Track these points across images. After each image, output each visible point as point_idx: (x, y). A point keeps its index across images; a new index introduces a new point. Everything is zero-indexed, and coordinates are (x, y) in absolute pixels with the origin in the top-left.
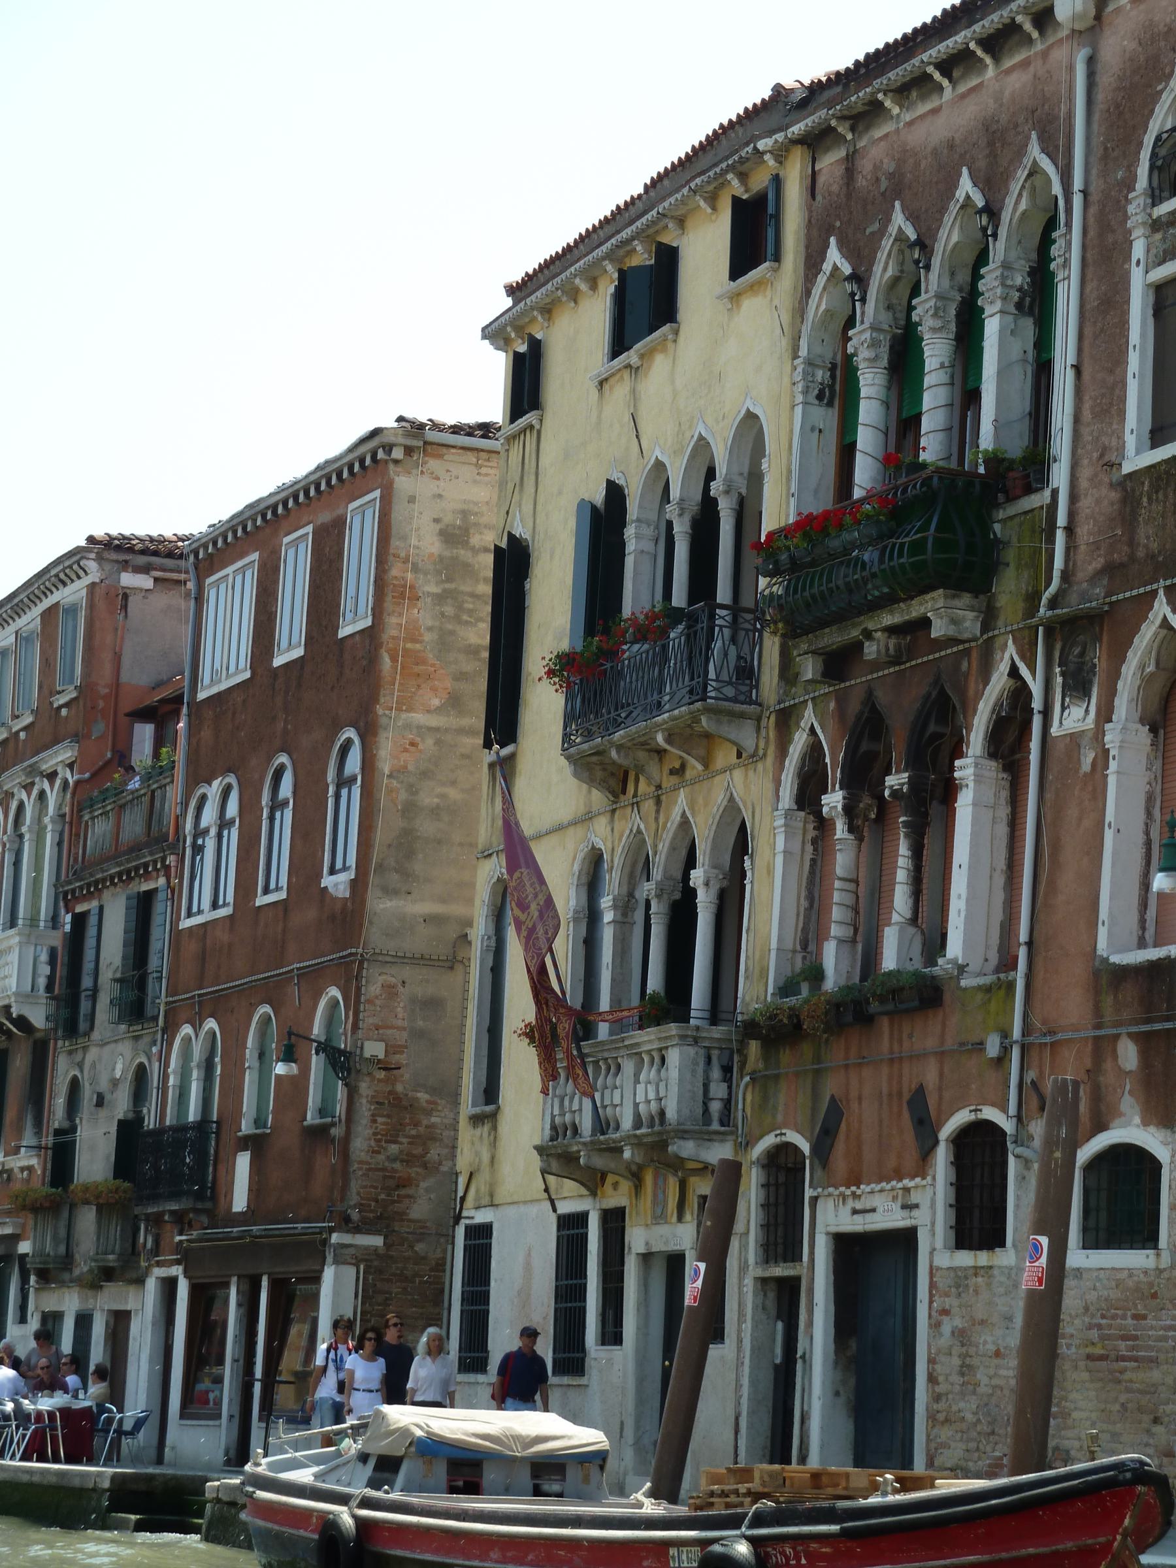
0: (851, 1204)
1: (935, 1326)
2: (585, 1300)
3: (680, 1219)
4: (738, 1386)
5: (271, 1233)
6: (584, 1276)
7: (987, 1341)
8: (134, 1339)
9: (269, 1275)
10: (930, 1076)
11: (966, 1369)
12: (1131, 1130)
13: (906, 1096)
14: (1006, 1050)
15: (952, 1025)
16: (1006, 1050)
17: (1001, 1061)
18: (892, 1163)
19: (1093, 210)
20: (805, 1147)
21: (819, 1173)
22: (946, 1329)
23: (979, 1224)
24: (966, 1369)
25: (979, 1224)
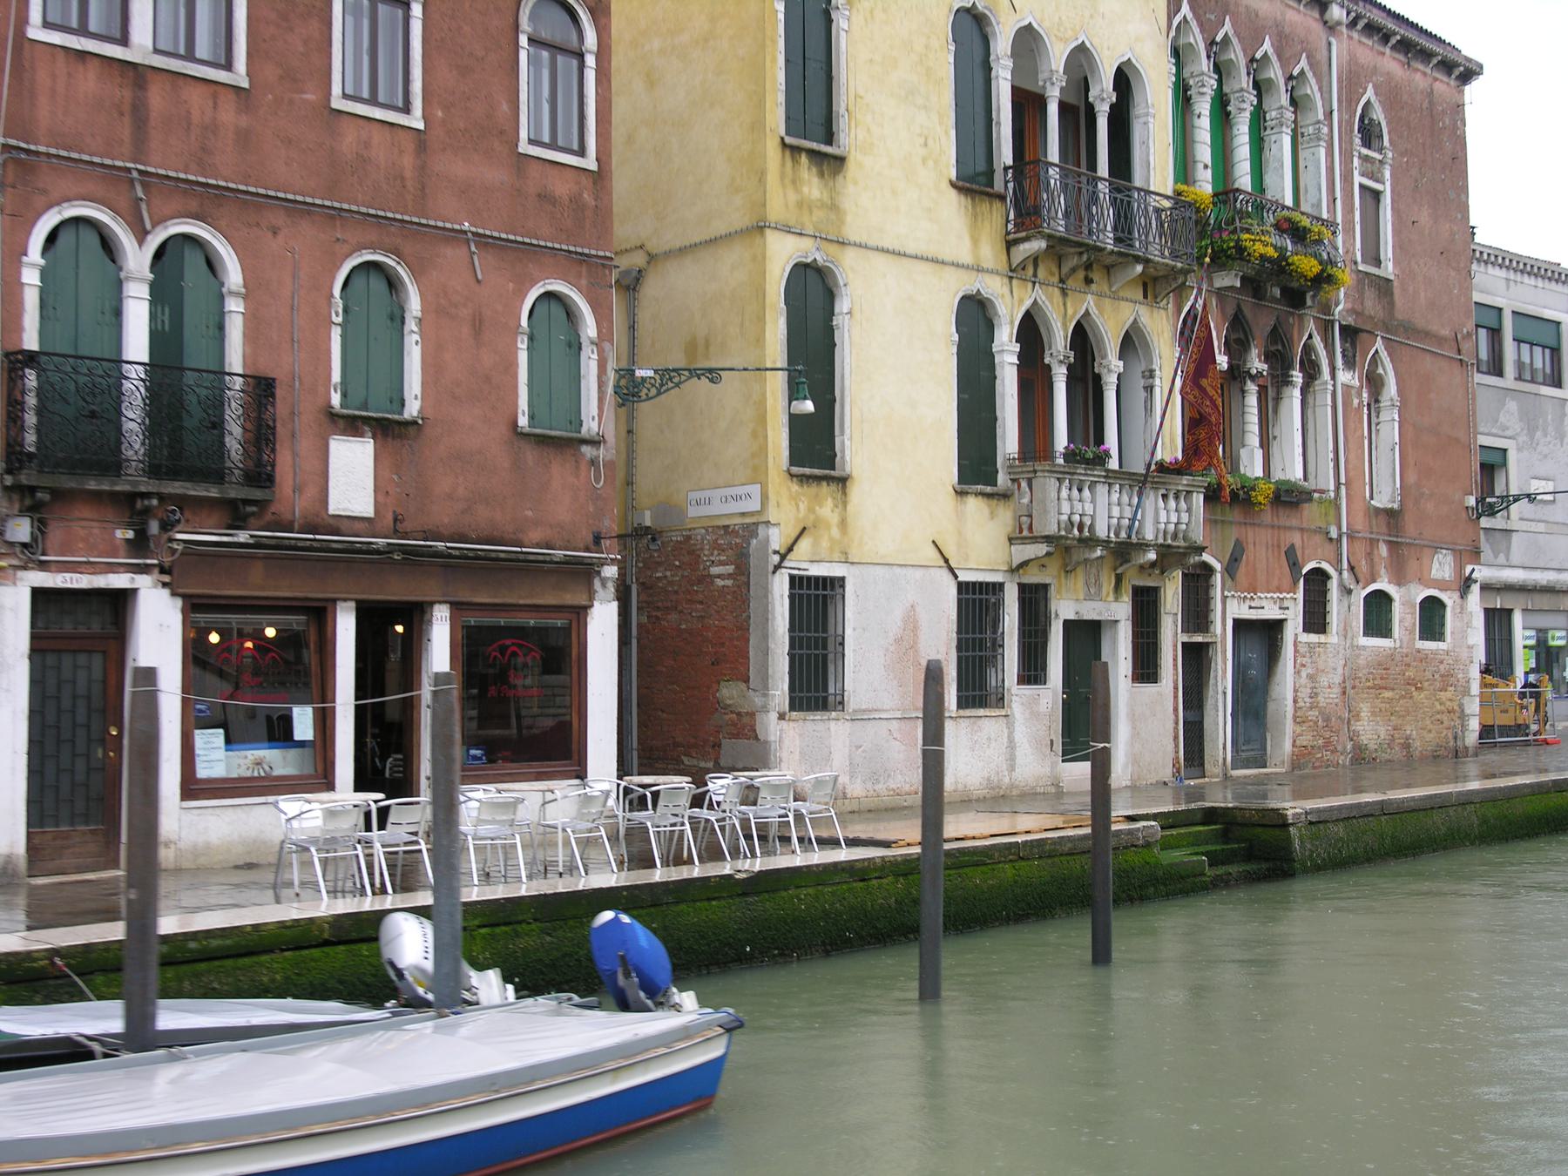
0: (1248, 603)
1: (1297, 673)
2: (959, 659)
3: (1116, 599)
4: (1176, 688)
5: (300, 544)
6: (360, 712)
7: (1323, 680)
8: (1100, 614)
9: (457, 607)
10: (1296, 539)
11: (1314, 695)
12: (1382, 585)
13: (1284, 549)
14: (1340, 536)
15: (1311, 514)
16: (1340, 536)
17: (1339, 540)
18: (1275, 583)
19: (1220, 690)
20: (1217, 566)
21: (1229, 582)
22: (1304, 674)
23: (1316, 620)
24: (1314, 695)
25: (1316, 620)
